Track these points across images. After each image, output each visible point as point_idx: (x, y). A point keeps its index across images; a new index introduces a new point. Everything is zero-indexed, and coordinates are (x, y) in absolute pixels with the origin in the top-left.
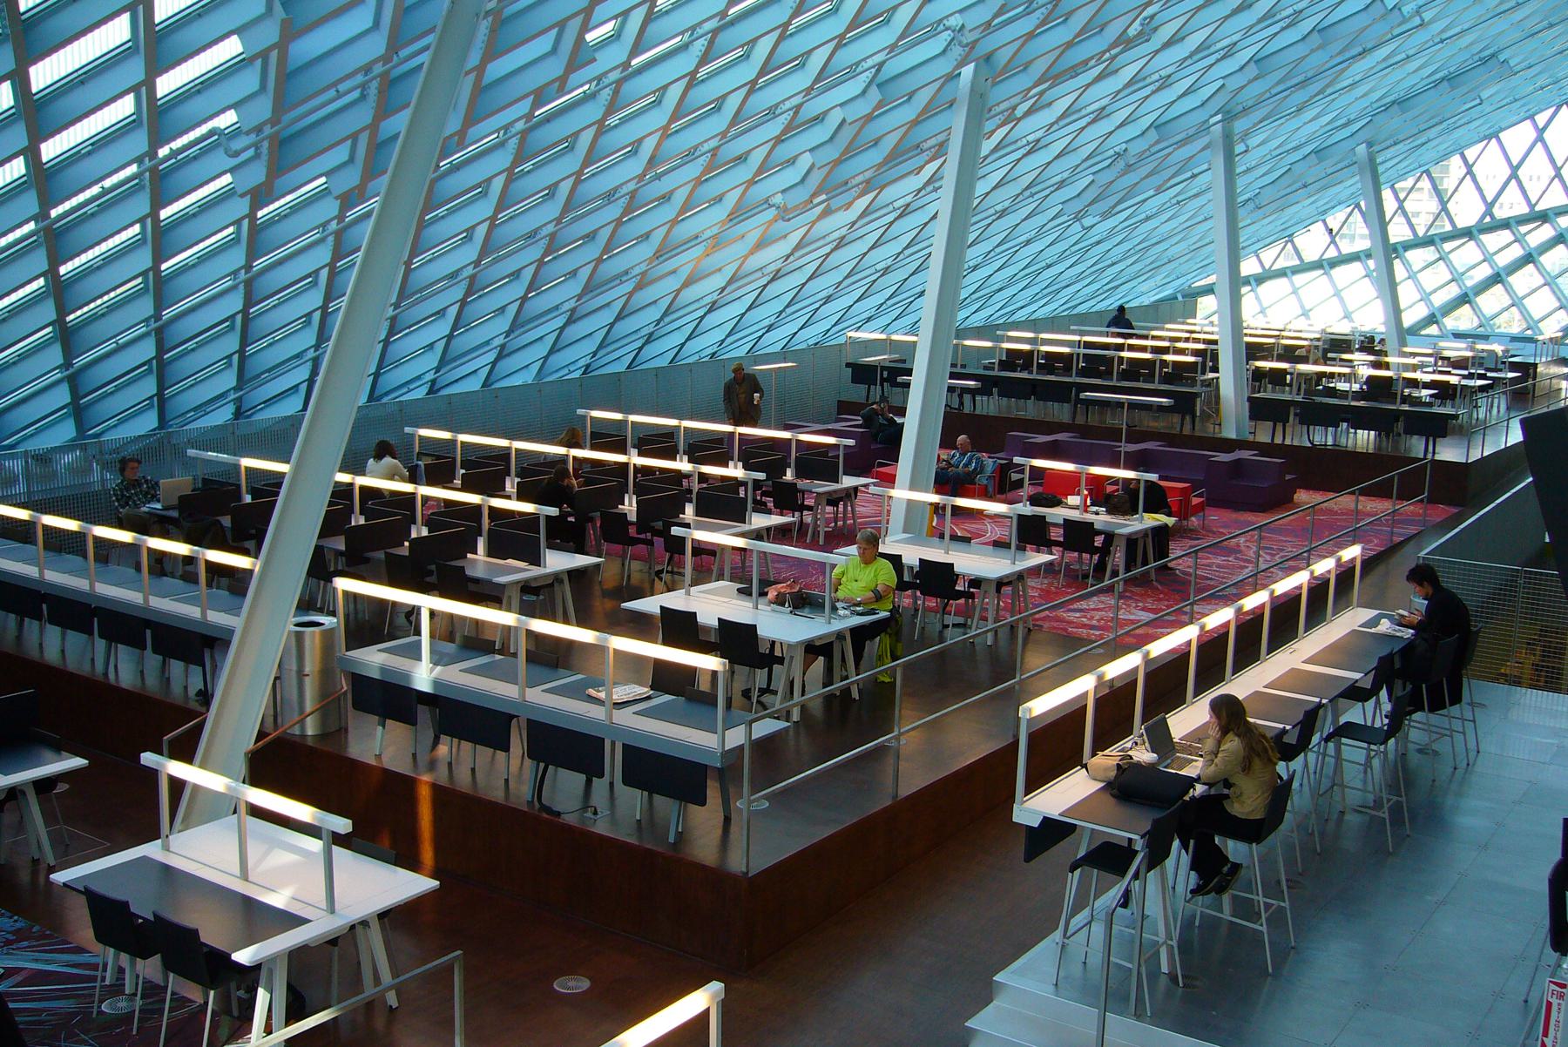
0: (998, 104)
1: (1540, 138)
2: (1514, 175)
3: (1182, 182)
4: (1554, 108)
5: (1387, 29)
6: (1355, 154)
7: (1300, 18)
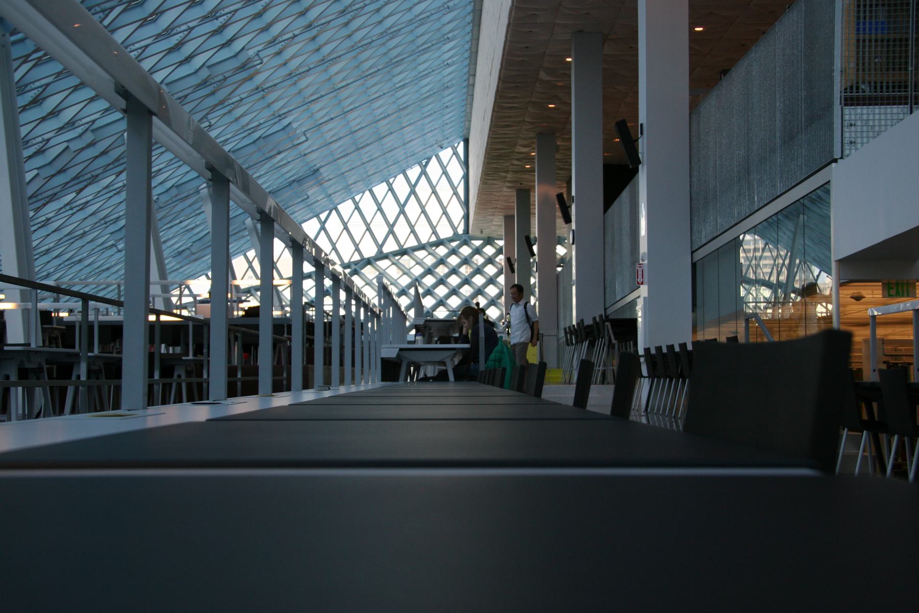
0: (216, 76)
1: (323, 228)
2: (402, 212)
3: (95, 253)
4: (328, 212)
5: (169, 198)
6: (244, 224)
7: (226, 143)
